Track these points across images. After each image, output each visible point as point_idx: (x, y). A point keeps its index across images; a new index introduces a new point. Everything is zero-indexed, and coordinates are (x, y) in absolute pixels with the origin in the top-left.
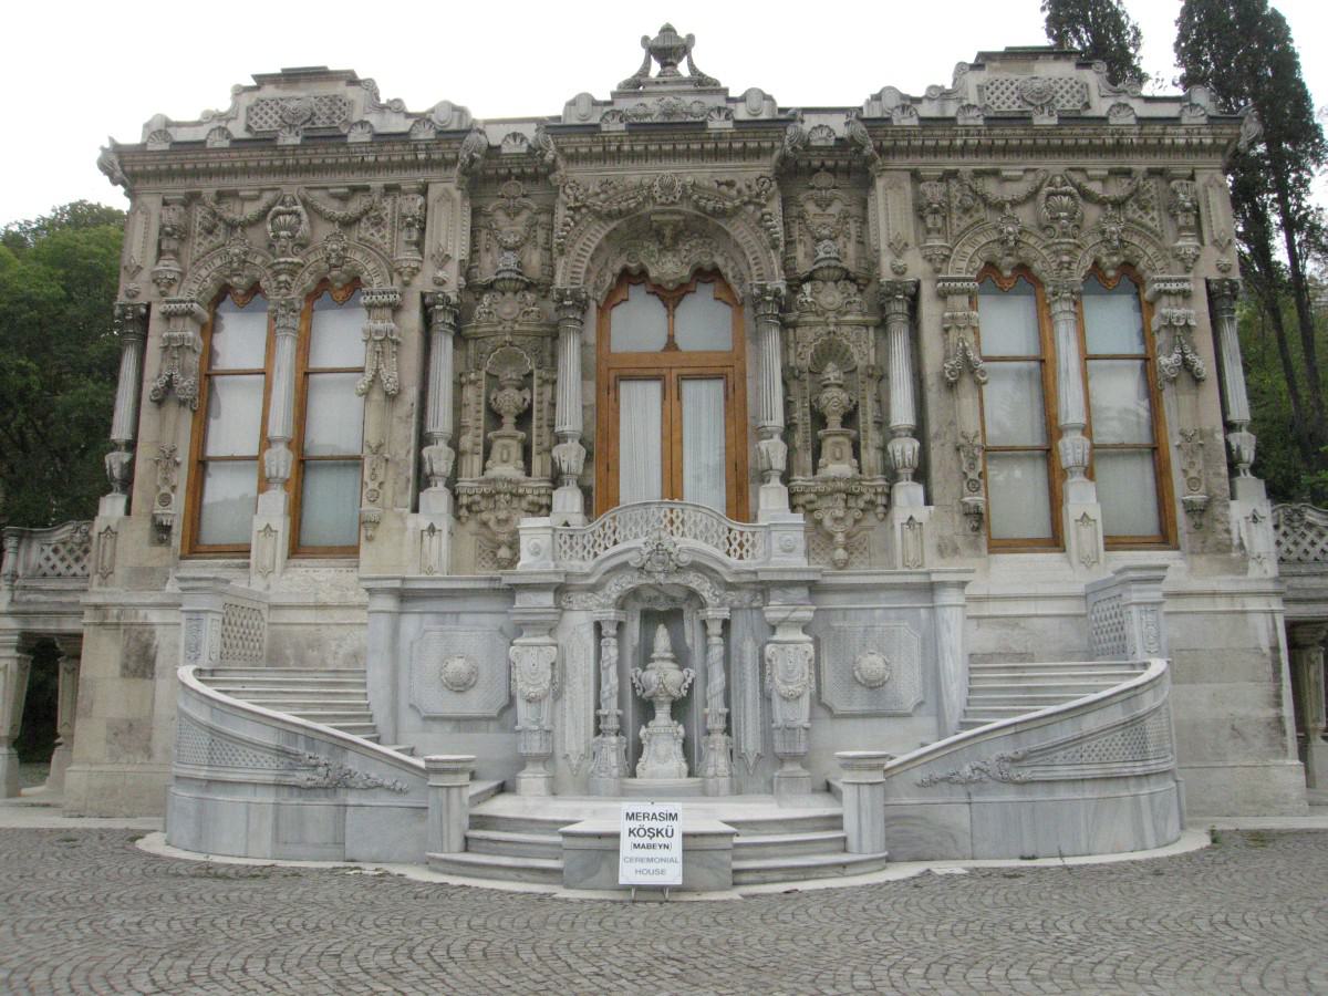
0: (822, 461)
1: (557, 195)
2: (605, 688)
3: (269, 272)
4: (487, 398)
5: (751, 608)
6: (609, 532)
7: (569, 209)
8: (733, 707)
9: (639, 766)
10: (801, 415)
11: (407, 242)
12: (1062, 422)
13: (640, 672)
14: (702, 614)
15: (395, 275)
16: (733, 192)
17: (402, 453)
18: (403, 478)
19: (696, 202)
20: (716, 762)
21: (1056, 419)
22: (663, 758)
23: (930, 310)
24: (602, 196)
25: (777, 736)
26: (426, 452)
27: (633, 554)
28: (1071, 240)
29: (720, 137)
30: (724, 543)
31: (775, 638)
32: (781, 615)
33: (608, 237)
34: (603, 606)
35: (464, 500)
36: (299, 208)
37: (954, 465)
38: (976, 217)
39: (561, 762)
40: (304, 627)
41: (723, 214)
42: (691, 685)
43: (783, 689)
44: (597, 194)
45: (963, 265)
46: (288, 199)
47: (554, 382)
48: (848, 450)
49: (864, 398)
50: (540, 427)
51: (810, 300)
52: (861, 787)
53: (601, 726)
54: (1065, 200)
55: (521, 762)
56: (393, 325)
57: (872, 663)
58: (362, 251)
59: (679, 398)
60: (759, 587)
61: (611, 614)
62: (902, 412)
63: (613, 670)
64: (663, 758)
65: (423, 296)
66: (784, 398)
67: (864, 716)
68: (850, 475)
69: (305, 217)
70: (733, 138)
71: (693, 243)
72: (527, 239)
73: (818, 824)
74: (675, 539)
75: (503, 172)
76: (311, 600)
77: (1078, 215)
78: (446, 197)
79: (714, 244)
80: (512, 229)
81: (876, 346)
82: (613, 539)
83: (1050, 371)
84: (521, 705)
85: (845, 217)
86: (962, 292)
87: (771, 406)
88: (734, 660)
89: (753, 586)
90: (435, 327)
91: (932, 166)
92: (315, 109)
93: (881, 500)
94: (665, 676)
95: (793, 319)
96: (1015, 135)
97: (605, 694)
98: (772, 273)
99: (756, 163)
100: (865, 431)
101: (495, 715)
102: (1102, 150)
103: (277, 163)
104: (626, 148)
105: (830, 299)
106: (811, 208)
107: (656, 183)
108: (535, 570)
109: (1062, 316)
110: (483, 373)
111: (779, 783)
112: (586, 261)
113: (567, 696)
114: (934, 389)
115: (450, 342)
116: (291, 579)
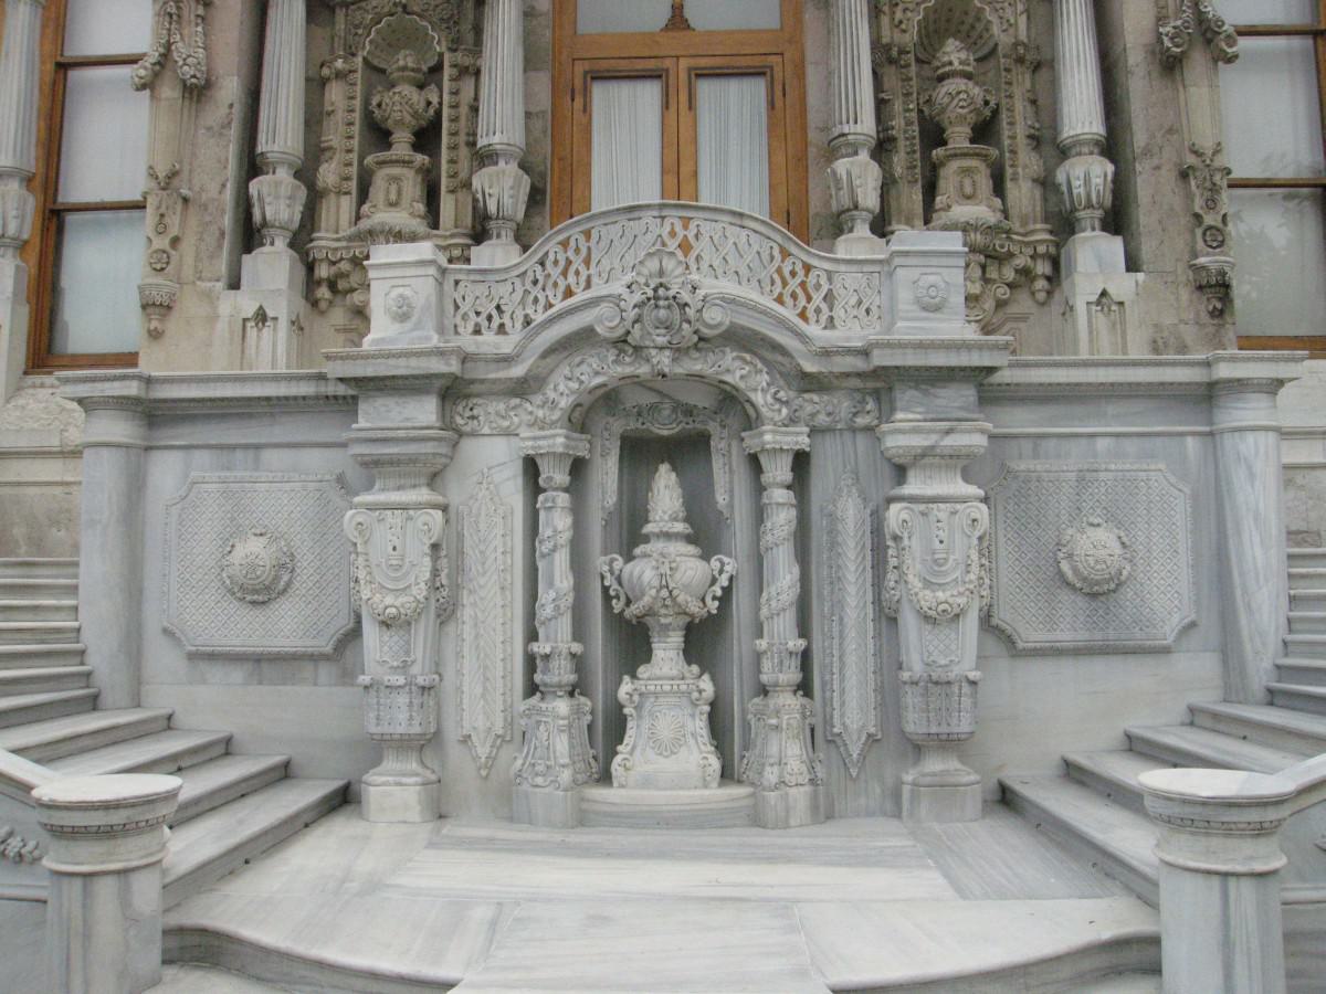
0: (940, 200)
2: (546, 596)
4: (366, 102)
6: (555, 272)
9: (618, 759)
10: (903, 123)
13: (619, 563)
14: (751, 442)
17: (213, 188)
18: (214, 229)
20: (783, 753)
22: (668, 749)
25: (911, 699)
26: (254, 186)
27: (604, 309)
30: (794, 296)
31: (907, 490)
32: (919, 441)
34: (541, 424)
35: (323, 271)
37: (1178, 202)
39: (454, 752)
40: (45, 490)
42: (727, 591)
43: (927, 598)
47: (478, 73)
48: (984, 183)
49: (1010, 97)
50: (453, 148)
52: (1232, 882)
53: (538, 678)
55: (377, 749)
57: (1096, 545)
59: (691, 106)
60: (870, 384)
61: (558, 440)
62: (1081, 113)
63: (562, 560)
64: (668, 749)
66: (876, 98)
67: (1077, 652)
73: (1086, 964)
74: (695, 277)
76: (54, 442)
82: (562, 287)
84: (370, 631)
88: (818, 538)
89: (856, 383)
93: (1043, 268)
94: (669, 571)
97: (545, 609)
100: (1013, 152)
101: (328, 649)
108: (400, 346)
111: (914, 797)
113: (467, 613)
116: (23, 407)
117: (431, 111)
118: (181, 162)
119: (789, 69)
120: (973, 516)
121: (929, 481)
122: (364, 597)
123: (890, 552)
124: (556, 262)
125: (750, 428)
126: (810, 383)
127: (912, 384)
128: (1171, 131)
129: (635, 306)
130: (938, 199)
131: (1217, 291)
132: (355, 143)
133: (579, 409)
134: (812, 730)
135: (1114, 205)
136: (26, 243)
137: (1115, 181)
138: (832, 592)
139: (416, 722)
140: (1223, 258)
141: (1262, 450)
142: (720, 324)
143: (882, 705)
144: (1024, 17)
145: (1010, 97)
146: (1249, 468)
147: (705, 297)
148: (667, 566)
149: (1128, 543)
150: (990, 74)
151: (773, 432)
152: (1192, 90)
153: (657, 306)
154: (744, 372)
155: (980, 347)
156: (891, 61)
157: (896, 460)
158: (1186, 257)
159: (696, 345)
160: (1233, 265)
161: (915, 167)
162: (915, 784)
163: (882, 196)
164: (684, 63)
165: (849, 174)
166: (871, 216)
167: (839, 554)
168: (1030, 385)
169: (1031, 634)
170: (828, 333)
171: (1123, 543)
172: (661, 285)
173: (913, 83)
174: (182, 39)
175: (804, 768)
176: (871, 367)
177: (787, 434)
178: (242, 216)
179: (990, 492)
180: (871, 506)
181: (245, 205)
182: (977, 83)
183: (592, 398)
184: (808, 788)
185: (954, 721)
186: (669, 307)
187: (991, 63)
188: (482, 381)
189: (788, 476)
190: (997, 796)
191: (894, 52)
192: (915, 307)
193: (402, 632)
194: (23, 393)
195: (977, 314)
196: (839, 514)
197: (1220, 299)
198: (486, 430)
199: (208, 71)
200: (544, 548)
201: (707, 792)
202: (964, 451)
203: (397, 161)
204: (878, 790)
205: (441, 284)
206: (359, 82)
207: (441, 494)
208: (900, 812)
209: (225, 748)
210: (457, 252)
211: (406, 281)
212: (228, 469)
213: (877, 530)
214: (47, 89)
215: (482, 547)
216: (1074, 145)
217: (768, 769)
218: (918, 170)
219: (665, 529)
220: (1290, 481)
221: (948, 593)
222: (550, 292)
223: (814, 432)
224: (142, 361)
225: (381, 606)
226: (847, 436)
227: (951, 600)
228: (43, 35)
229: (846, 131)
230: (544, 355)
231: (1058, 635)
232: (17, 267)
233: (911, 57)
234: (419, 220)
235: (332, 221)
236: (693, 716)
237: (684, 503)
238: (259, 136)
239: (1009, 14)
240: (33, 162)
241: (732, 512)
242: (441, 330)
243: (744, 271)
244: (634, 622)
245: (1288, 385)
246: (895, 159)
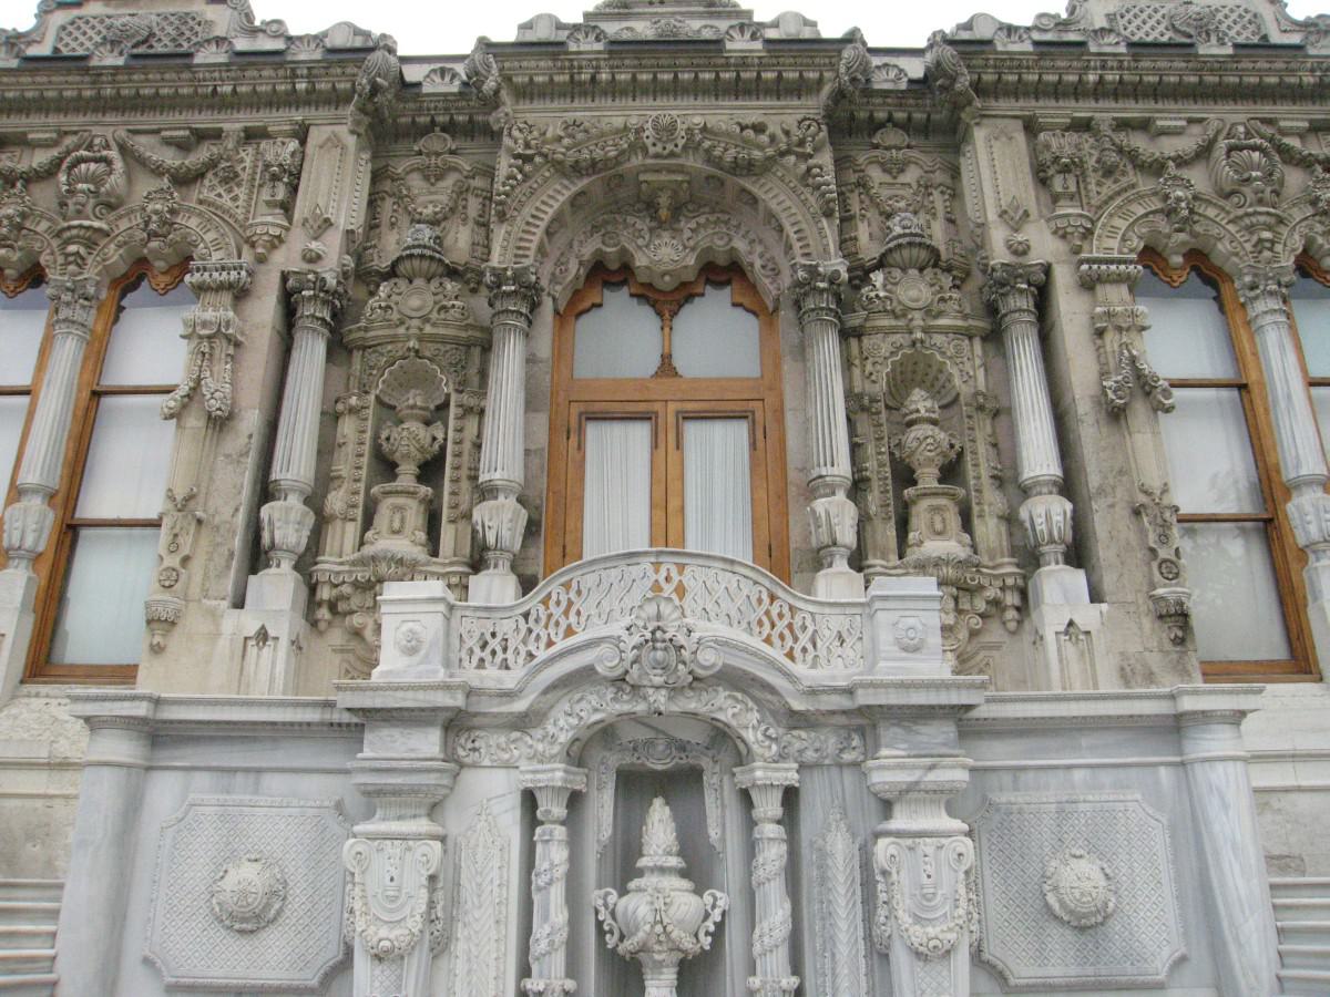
2: (540, 930)
3: (55, 243)
4: (376, 437)
5: (841, 766)
6: (557, 612)
11: (268, 203)
12: (1289, 474)
13: (613, 897)
16: (764, 138)
17: (227, 512)
18: (224, 550)
19: (708, 151)
21: (1278, 472)
23: (1070, 308)
24: (566, 141)
26: (265, 511)
27: (605, 650)
28: (1272, 210)
29: (743, 62)
30: (782, 637)
31: (894, 825)
32: (904, 777)
33: (575, 202)
35: (325, 593)
36: (114, 154)
37: (1133, 538)
38: (1124, 181)
40: (29, 803)
41: (748, 168)
42: (720, 926)
43: (918, 935)
44: (560, 139)
45: (1114, 244)
46: (97, 141)
47: (482, 412)
48: (954, 521)
49: (973, 441)
50: (455, 481)
54: (1256, 155)
56: (231, 314)
57: (1080, 878)
58: (200, 214)
59: (679, 446)
60: (859, 721)
61: (556, 774)
62: (1039, 456)
63: (557, 894)
65: (285, 277)
69: (119, 165)
70: (762, 65)
71: (702, 220)
72: (452, 210)
74: (689, 620)
75: (423, 120)
76: (42, 754)
77: (1276, 176)
78: (334, 142)
79: (734, 222)
80: (430, 198)
81: (984, 365)
83: (1258, 402)
84: (362, 965)
85: (926, 188)
88: (809, 873)
89: (843, 720)
90: (300, 323)
91: (1053, 111)
92: (156, 30)
93: (1012, 599)
96: (1174, 71)
97: (539, 946)
98: (826, 250)
99: (796, 102)
100: (979, 491)
101: (314, 982)
102: (1297, 94)
103: (87, 93)
104: (604, 76)
105: (913, 293)
106: (876, 175)
107: (649, 125)
108: (409, 679)
109: (1269, 319)
110: (372, 398)
112: (539, 232)
113: (460, 947)
114: (1090, 420)
116: (16, 718)
117: (436, 446)
118: (198, 486)
119: (769, 415)
120: (959, 850)
121: (914, 816)
122: (359, 930)
123: (880, 887)
124: (558, 603)
125: (741, 764)
127: (895, 721)
128: (1121, 472)
129: (634, 648)
130: (911, 535)
131: (1178, 620)
132: (364, 473)
133: (577, 743)
135: (1074, 538)
136: (40, 554)
137: (1073, 518)
138: (824, 927)
140: (1179, 589)
142: (713, 665)
144: (982, 370)
146: (1222, 798)
147: (700, 639)
148: (661, 900)
149: (1112, 875)
150: (955, 419)
151: (765, 768)
153: (654, 648)
154: (736, 710)
155: (958, 686)
156: (863, 409)
158: (1145, 589)
161: (888, 505)
163: (858, 533)
164: (672, 407)
166: (849, 552)
167: (830, 890)
171: (1106, 875)
172: (659, 628)
174: (212, 375)
176: (856, 705)
177: (777, 770)
179: (975, 826)
180: (859, 840)
181: (255, 528)
182: (942, 428)
183: (591, 732)
186: (665, 649)
188: (485, 714)
189: (778, 811)
191: (866, 401)
192: (896, 648)
193: (394, 967)
194: (16, 701)
196: (829, 848)
197: (1181, 628)
198: (487, 762)
202: (947, 786)
203: (402, 492)
206: (371, 417)
207: (440, 825)
210: (454, 580)
211: (416, 617)
212: (228, 792)
213: (866, 864)
214: (80, 413)
215: (479, 880)
218: (891, 508)
219: (659, 864)
220: (1267, 804)
221: (938, 929)
222: (552, 631)
223: (803, 767)
225: (375, 940)
226: (835, 771)
227: (941, 937)
228: (83, 367)
229: (824, 473)
230: (546, 692)
232: (29, 579)
233: (882, 404)
234: (420, 548)
235: (337, 544)
237: (677, 837)
238: (275, 463)
239: (968, 367)
240: (57, 480)
241: (724, 847)
242: (447, 664)
243: (733, 613)
244: (628, 957)
245: (1250, 716)
246: (870, 498)
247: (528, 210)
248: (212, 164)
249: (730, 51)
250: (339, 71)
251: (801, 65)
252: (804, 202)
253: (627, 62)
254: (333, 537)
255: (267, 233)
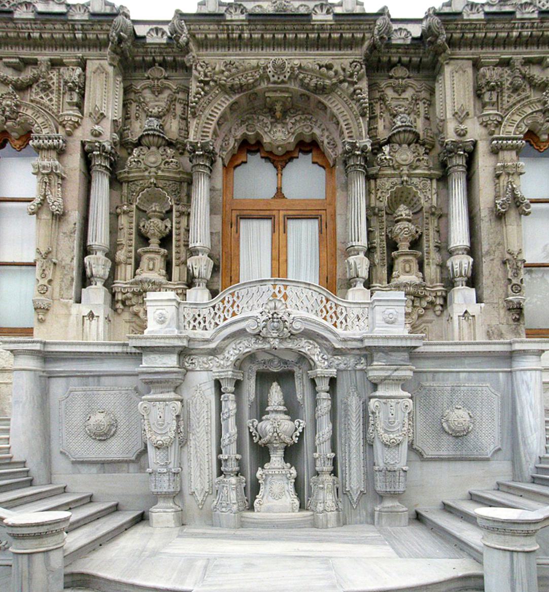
1: (191, 74)
2: (225, 436)
4: (138, 225)
6: (228, 306)
7: (201, 82)
8: (339, 451)
9: (257, 501)
10: (379, 241)
11: (69, 103)
15: (60, 128)
16: (332, 73)
17: (68, 260)
18: (69, 277)
19: (301, 80)
20: (325, 498)
22: (277, 494)
23: (484, 164)
25: (379, 477)
26: (87, 259)
27: (250, 322)
29: (322, 28)
30: (331, 317)
31: (377, 393)
33: (232, 107)
35: (119, 297)
37: (501, 274)
38: (523, 95)
39: (188, 498)
41: (322, 90)
42: (302, 434)
43: (386, 437)
44: (223, 72)
45: (512, 129)
47: (189, 214)
48: (415, 267)
49: (428, 230)
51: (388, 157)
53: (222, 469)
55: (155, 498)
56: (57, 163)
57: (459, 417)
58: (33, 108)
59: (285, 232)
62: (459, 236)
63: (232, 421)
64: (277, 494)
65: (83, 144)
67: (449, 460)
68: (418, 282)
70: (332, 30)
71: (298, 118)
72: (168, 111)
74: (289, 310)
78: (100, 70)
80: (156, 104)
81: (437, 193)
82: (231, 312)
85: (416, 100)
86: (512, 148)
87: (357, 231)
89: (358, 352)
93: (439, 301)
94: (277, 425)
95: (375, 172)
99: (349, 52)
101: (133, 458)
105: (404, 157)
106: (390, 93)
110: (134, 206)
111: (380, 516)
112: (214, 123)
114: (487, 219)
115: (106, 181)
117: (167, 230)
118: (52, 247)
119: (329, 217)
124: (229, 302)
126: (337, 352)
128: (499, 244)
130: (394, 273)
131: (517, 311)
132: (133, 242)
134: (337, 489)
135: (472, 275)
139: (171, 487)
141: (533, 378)
142: (300, 329)
143: (366, 480)
145: (428, 230)
146: (528, 386)
152: (509, 227)
153: (273, 322)
156: (375, 214)
157: (373, 381)
159: (289, 337)
160: (524, 300)
162: (380, 511)
163: (369, 272)
164: (282, 213)
165: (355, 263)
168: (432, 352)
169: (430, 452)
170: (345, 332)
173: (385, 223)
174: (51, 193)
175: (334, 504)
178: (81, 272)
181: (83, 268)
182: (413, 224)
184: (336, 512)
185: (397, 486)
186: (278, 322)
187: (420, 214)
188: (197, 349)
189: (328, 388)
190: (415, 517)
191: (376, 210)
195: (409, 320)
197: (518, 314)
198: (198, 369)
199: (64, 208)
200: (224, 417)
201: (294, 514)
204: (365, 513)
205: (178, 309)
208: (374, 521)
209: (90, 499)
210: (180, 291)
211: (163, 307)
213: (365, 409)
216: (456, 250)
217: (319, 505)
218: (385, 261)
222: (226, 314)
224: (35, 332)
230: (224, 340)
231: (441, 453)
233: (384, 212)
235: (123, 275)
236: (288, 483)
242: (178, 328)
243: (309, 307)
247: (207, 112)
248: (35, 80)
249: (315, 21)
250: (99, 27)
251: (353, 29)
252: (351, 109)
253: (258, 27)
254: (121, 272)
255: (71, 120)
